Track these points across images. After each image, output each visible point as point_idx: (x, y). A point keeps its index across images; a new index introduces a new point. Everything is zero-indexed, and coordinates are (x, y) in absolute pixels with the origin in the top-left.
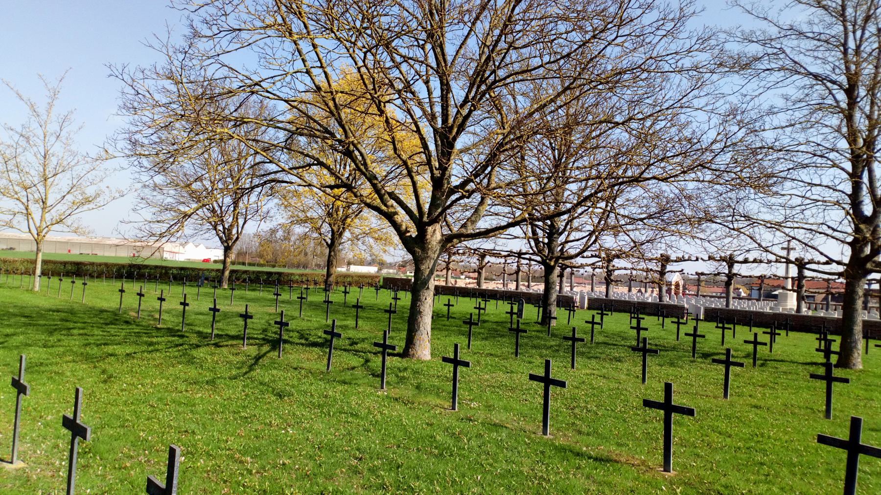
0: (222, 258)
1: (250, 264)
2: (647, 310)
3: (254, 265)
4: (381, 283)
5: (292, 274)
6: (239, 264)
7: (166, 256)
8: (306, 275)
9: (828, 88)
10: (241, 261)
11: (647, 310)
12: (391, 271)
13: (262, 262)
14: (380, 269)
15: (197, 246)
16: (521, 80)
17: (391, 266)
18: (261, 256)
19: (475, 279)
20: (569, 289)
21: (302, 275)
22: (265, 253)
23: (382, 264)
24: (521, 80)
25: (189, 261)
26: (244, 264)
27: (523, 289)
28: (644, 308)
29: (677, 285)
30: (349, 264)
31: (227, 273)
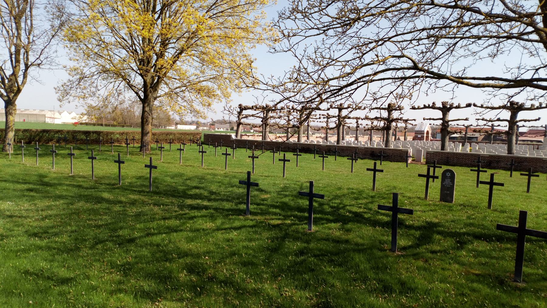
0: (441, 117)
1: (106, 125)
2: (502, 164)
3: (109, 126)
4: (202, 139)
5: (112, 133)
6: (98, 125)
7: (48, 121)
8: (127, 134)
9: (420, 70)
10: (100, 123)
11: (502, 164)
12: (205, 128)
13: (115, 123)
14: (197, 127)
15: (70, 113)
16: (398, 69)
17: (204, 125)
18: (114, 119)
19: (260, 132)
20: (306, 138)
21: (122, 134)
22: (117, 118)
23: (198, 124)
24: (398, 69)
25: (64, 124)
26: (102, 125)
27: (303, 140)
28: (498, 162)
29: (428, 132)
30: (177, 124)
31: (11, 135)
